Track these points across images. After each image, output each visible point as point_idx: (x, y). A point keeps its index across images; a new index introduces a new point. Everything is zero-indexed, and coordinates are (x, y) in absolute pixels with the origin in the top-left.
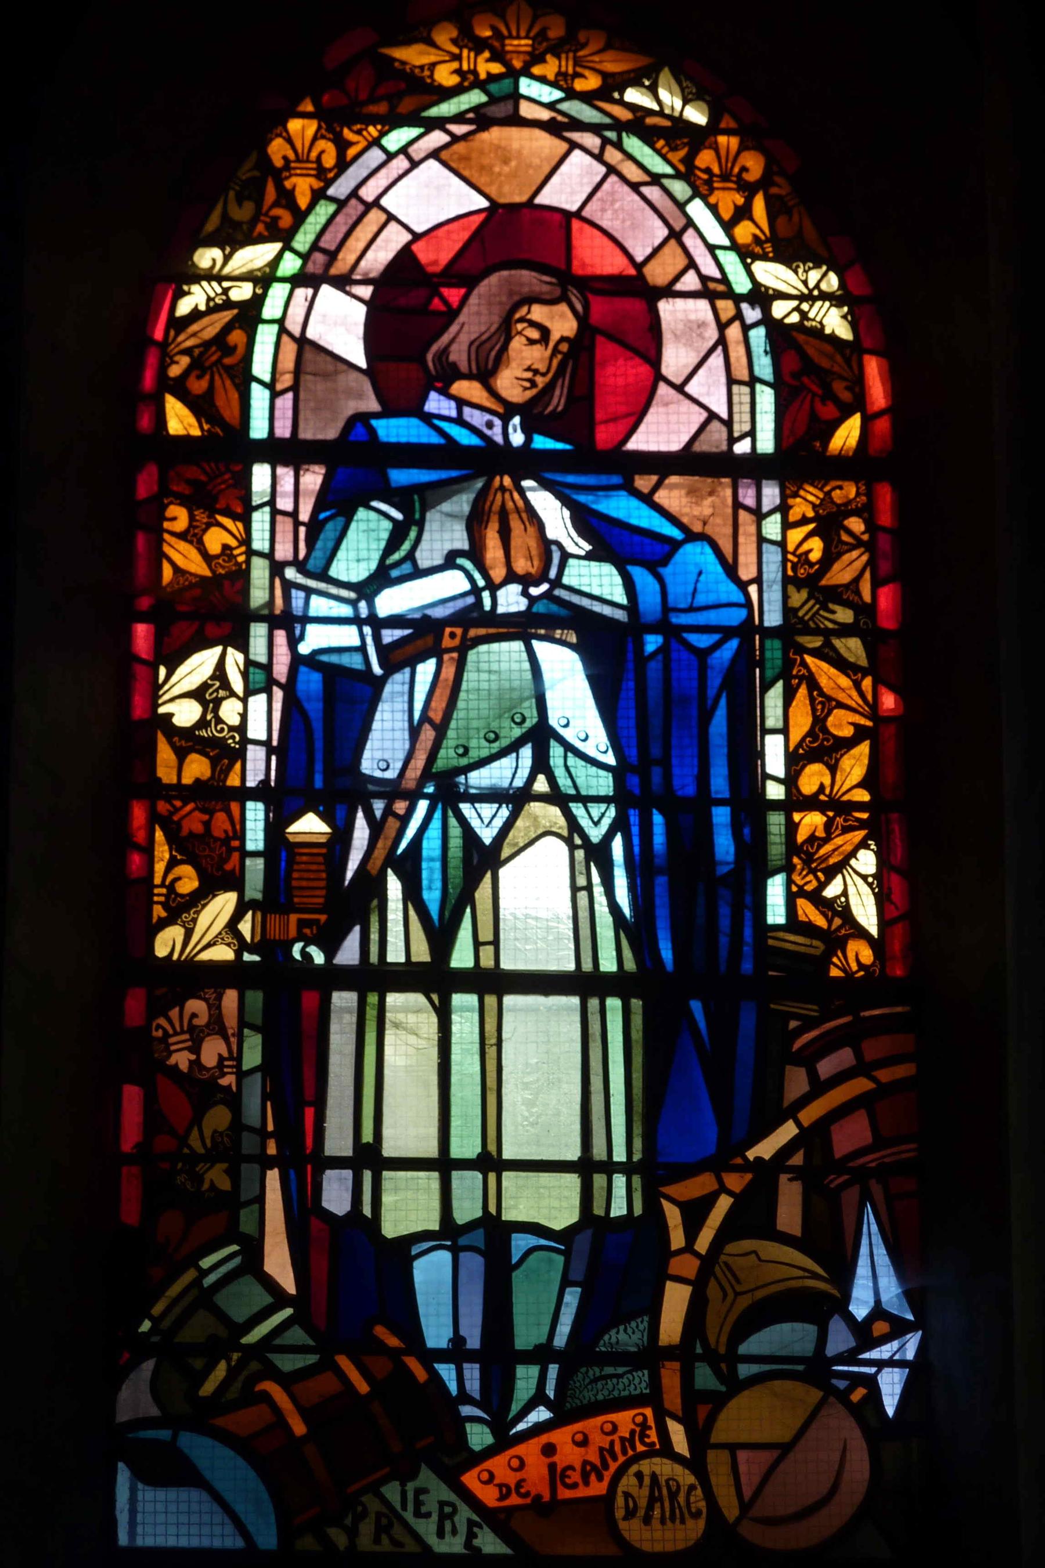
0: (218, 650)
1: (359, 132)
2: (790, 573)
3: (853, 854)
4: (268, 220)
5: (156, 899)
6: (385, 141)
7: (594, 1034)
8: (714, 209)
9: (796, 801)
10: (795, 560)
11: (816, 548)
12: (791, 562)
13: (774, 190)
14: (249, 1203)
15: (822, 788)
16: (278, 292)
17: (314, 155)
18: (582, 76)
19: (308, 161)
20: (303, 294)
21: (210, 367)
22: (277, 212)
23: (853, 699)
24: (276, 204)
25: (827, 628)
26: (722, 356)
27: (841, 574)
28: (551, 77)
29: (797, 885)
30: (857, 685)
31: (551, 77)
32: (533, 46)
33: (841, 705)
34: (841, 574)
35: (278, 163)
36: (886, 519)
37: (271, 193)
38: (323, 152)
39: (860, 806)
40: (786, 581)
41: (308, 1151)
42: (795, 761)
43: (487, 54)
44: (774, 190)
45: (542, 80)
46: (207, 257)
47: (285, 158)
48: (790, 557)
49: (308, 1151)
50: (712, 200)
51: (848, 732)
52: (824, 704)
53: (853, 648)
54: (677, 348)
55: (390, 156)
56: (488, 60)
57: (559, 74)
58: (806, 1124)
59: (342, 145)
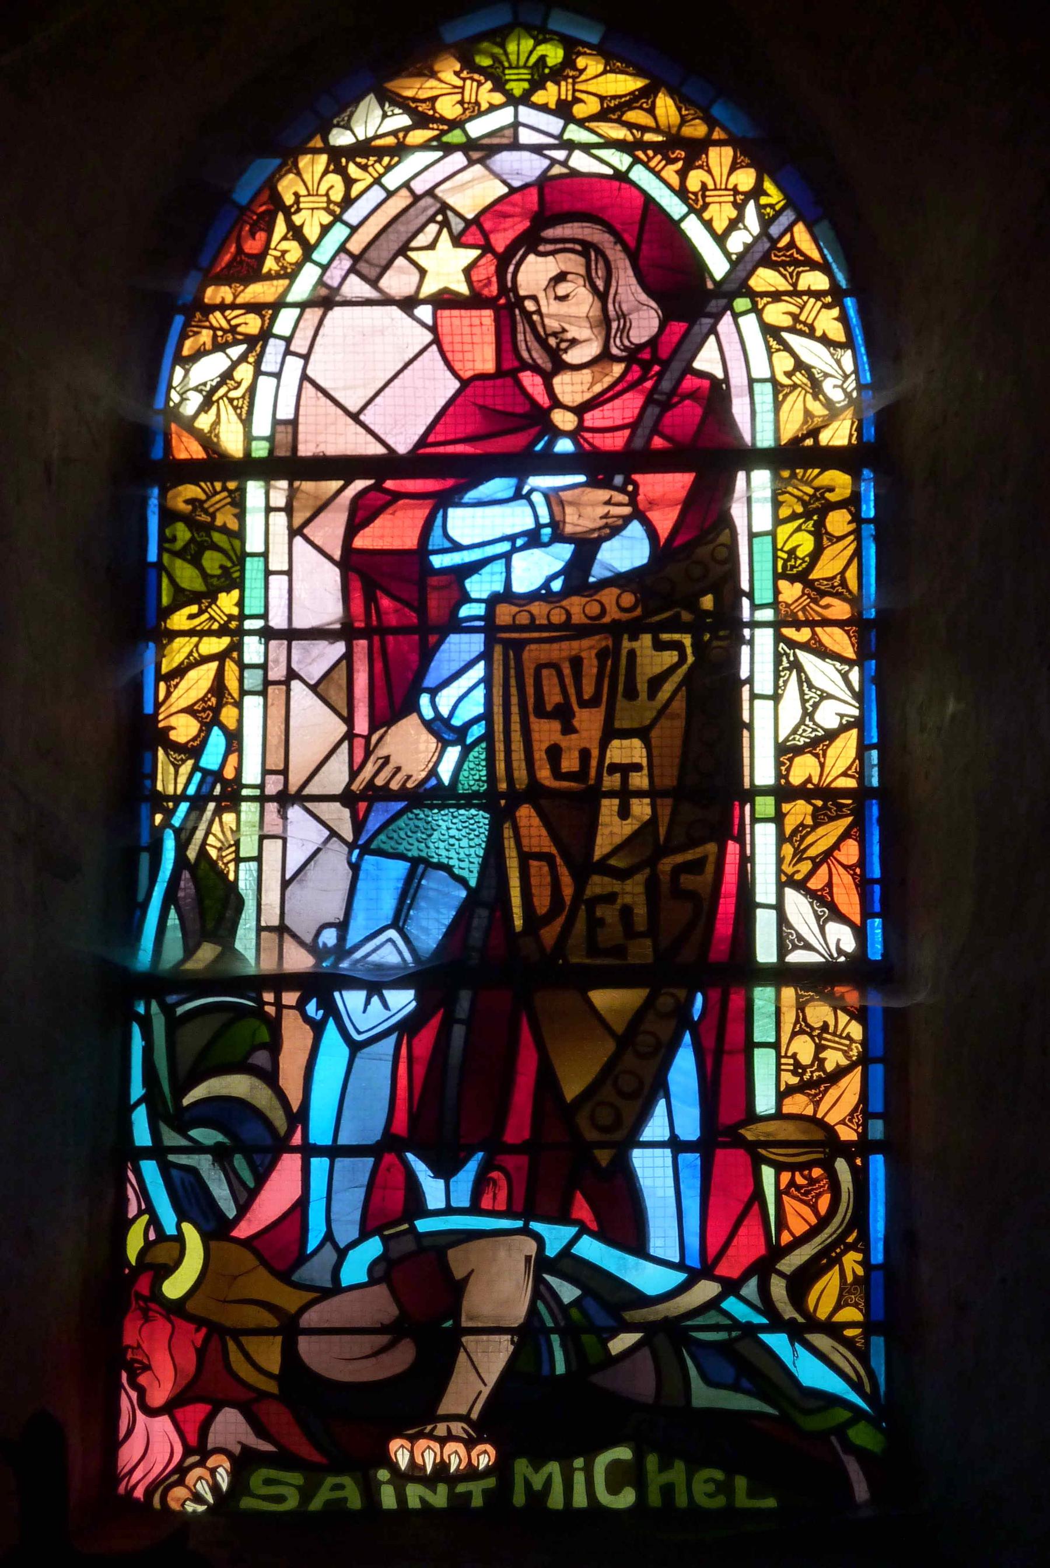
1: (364, 168)
2: (780, 570)
3: (836, 846)
5: (245, 792)
6: (346, 217)
8: (708, 225)
10: (785, 556)
11: (805, 543)
13: (764, 200)
14: (709, 315)
15: (809, 780)
18: (581, 101)
20: (313, 315)
21: (217, 401)
22: (285, 245)
26: (251, 1338)
27: (826, 569)
28: (552, 105)
29: (786, 874)
30: (845, 676)
31: (552, 105)
34: (826, 569)
35: (289, 200)
36: (869, 510)
39: (845, 792)
40: (777, 577)
42: (785, 752)
44: (764, 200)
45: (544, 108)
46: (214, 294)
48: (780, 553)
50: (706, 216)
51: (833, 723)
53: (838, 640)
54: (398, 880)
55: (390, 194)
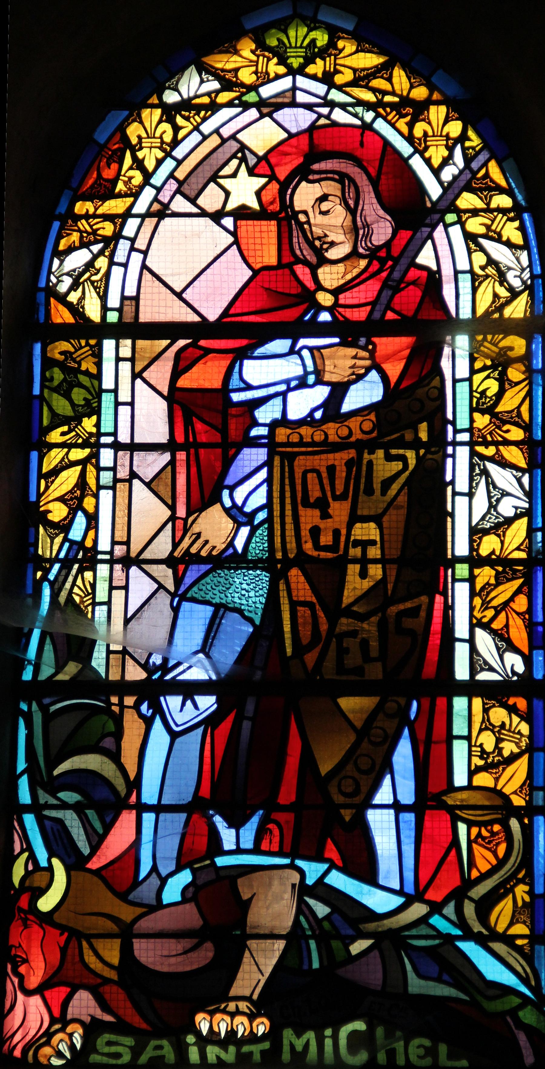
0: (258, 622)
1: (187, 119)
4: (126, 179)
7: (538, 862)
8: (428, 162)
9: (475, 561)
10: (478, 396)
11: (493, 387)
12: (476, 397)
15: (493, 552)
16: (130, 227)
17: (158, 134)
19: (154, 137)
23: (514, 489)
24: (131, 168)
25: (498, 440)
27: (509, 403)
30: (519, 480)
32: (306, 52)
33: (502, 542)
34: (509, 403)
35: (134, 141)
37: (128, 161)
38: (164, 132)
39: (519, 561)
41: (261, 812)
43: (275, 60)
44: (467, 144)
45: (314, 77)
47: (140, 137)
48: (475, 394)
49: (261, 812)
51: (510, 513)
52: (496, 495)
53: (515, 455)
56: (277, 64)
57: (325, 72)
58: (411, 161)
59: (176, 129)
